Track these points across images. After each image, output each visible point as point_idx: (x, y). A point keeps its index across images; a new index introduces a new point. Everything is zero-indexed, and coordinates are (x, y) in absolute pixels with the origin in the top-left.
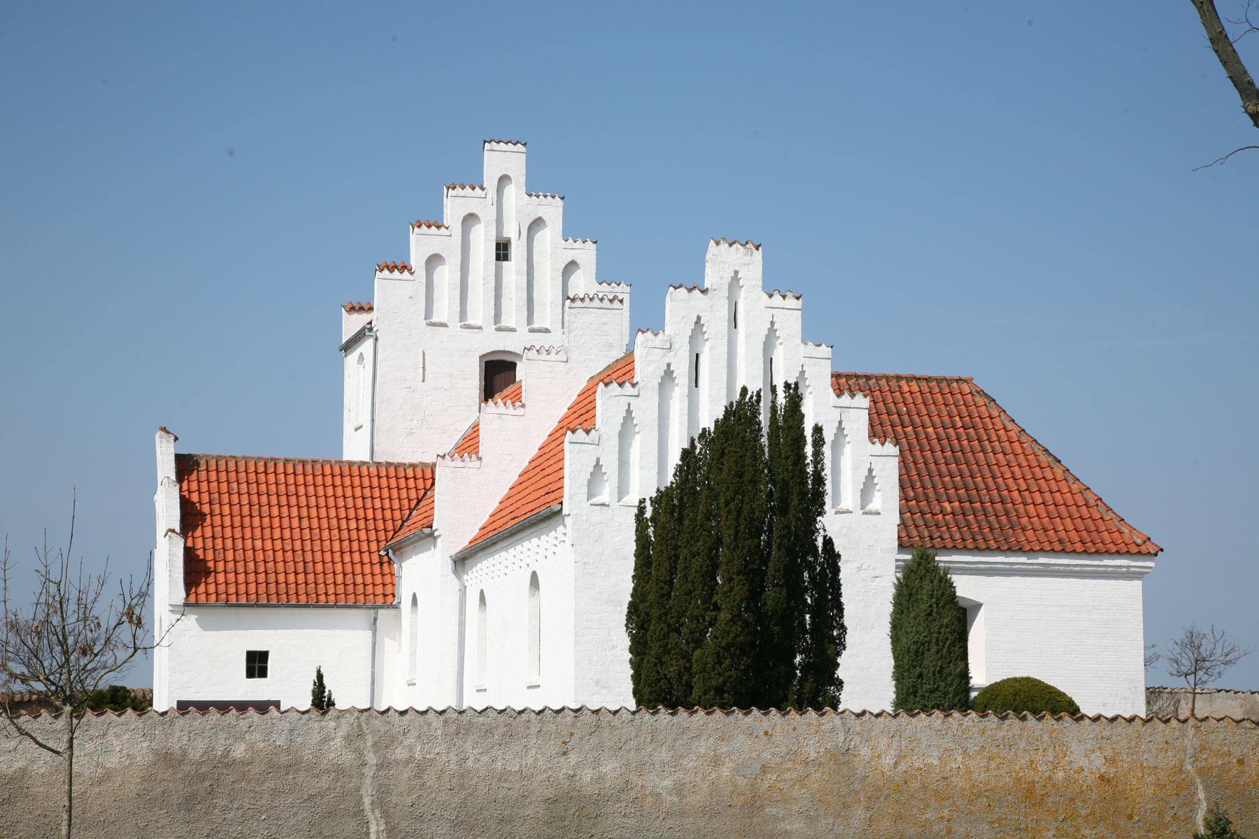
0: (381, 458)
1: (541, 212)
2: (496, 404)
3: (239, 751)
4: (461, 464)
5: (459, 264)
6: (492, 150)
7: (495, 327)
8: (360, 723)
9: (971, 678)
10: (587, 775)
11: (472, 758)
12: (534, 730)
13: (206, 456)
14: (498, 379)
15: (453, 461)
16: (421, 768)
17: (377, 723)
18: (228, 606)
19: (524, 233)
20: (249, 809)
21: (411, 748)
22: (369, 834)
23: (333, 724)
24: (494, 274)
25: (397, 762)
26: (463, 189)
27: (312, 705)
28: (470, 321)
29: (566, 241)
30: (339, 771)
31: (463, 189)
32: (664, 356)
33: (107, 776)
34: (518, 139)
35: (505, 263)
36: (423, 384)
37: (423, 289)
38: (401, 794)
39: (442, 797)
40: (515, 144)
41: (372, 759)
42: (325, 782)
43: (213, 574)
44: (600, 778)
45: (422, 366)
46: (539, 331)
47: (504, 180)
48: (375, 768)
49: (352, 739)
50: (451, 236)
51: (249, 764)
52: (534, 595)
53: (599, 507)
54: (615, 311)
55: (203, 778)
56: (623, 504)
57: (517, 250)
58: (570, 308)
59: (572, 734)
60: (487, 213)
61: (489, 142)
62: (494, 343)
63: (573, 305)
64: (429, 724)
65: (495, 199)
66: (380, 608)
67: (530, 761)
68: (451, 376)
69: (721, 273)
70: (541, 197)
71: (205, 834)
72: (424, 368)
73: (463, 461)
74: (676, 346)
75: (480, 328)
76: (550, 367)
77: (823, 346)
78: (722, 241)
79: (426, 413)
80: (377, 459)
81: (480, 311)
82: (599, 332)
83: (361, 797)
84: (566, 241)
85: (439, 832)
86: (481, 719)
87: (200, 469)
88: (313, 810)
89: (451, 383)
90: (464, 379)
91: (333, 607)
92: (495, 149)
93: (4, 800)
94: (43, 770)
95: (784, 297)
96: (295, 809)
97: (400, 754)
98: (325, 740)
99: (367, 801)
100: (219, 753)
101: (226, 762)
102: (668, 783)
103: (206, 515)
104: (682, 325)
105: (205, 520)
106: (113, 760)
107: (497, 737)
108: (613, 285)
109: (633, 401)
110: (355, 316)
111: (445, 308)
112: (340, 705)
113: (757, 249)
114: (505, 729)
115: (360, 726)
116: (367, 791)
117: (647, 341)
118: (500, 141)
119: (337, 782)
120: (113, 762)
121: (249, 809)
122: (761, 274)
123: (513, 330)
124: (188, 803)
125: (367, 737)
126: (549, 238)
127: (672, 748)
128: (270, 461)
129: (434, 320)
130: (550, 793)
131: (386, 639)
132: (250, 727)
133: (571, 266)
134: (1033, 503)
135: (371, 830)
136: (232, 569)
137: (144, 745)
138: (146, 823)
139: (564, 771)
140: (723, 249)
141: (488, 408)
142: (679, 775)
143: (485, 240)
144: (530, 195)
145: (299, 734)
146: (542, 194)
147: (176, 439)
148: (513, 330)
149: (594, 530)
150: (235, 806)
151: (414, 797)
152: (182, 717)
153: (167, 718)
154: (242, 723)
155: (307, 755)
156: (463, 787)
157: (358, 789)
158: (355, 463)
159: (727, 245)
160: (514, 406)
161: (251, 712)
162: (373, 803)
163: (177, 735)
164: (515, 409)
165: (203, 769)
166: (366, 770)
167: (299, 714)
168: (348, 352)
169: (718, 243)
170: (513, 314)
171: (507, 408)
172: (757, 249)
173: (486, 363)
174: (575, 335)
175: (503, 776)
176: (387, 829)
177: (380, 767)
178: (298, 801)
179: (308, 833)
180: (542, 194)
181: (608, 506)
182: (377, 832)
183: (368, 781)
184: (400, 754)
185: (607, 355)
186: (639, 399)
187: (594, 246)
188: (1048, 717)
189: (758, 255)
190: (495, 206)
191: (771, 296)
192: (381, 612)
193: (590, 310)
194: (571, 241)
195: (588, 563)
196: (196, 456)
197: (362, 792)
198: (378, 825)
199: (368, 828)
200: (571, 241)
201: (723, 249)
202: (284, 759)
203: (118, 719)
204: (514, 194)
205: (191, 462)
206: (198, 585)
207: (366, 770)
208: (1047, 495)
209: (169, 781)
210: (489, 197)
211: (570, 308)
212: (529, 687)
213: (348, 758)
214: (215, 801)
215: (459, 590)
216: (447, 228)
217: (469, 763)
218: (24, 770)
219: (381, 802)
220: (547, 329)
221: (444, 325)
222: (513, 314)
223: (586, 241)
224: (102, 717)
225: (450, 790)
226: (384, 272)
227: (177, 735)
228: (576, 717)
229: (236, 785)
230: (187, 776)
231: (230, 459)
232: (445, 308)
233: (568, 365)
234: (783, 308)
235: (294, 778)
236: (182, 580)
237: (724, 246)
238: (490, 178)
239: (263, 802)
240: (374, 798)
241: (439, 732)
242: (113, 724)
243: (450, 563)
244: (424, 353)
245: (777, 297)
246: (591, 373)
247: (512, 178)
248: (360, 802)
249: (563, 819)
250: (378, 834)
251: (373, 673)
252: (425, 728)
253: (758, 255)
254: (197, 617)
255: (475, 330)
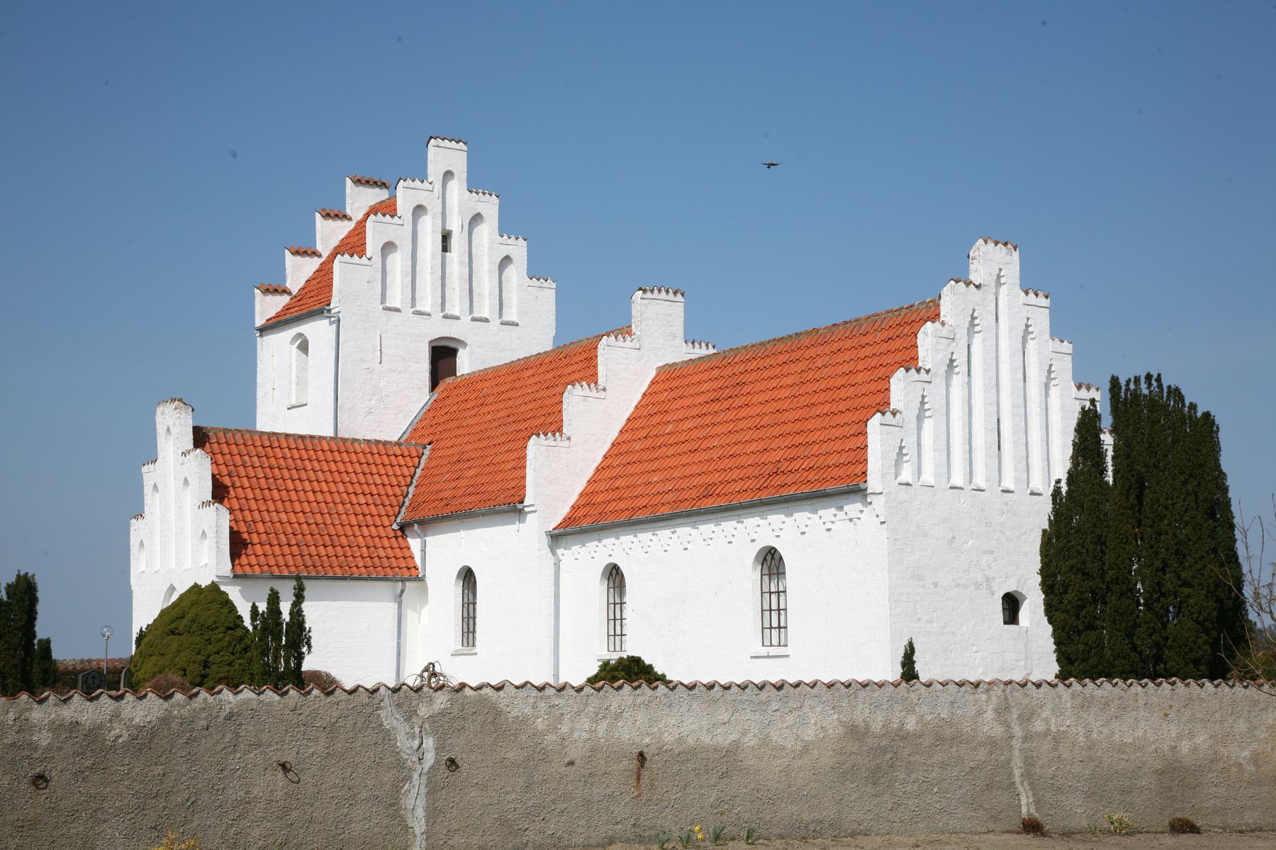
0: (343, 434)
1: (480, 208)
2: (582, 386)
3: (911, 724)
4: (554, 443)
5: (411, 252)
6: (438, 146)
7: (442, 314)
8: (1005, 696)
9: (1054, 652)
10: (1185, 746)
11: (1095, 730)
12: (1141, 703)
13: (214, 429)
14: (442, 364)
15: (546, 440)
16: (1057, 739)
17: (1019, 694)
18: (273, 578)
19: (466, 228)
20: (923, 782)
21: (1047, 720)
22: (1021, 806)
23: (984, 697)
24: (440, 264)
25: (1038, 735)
26: (413, 181)
27: (902, 677)
28: (448, 311)
29: (502, 237)
30: (992, 743)
31: (413, 181)
32: (949, 345)
33: (807, 748)
34: (438, 135)
35: (448, 254)
36: (380, 366)
37: (379, 275)
38: (1042, 767)
39: (1077, 768)
40: (457, 142)
41: (1018, 731)
42: (982, 754)
43: (250, 546)
44: (1195, 749)
45: (379, 348)
46: (480, 320)
47: (448, 175)
48: (1020, 740)
49: (1003, 710)
50: (403, 225)
51: (920, 737)
52: (756, 569)
53: (904, 487)
54: (678, 303)
55: (884, 750)
56: (922, 484)
57: (457, 242)
58: (642, 298)
59: (1171, 707)
60: (434, 206)
61: (435, 139)
62: (441, 329)
63: (645, 296)
64: (1060, 697)
65: (441, 193)
66: (408, 580)
67: (1141, 733)
68: (405, 359)
69: (990, 270)
70: (481, 194)
71: (890, 808)
72: (381, 350)
73: (555, 440)
74: (958, 336)
75: (429, 315)
76: (626, 353)
77: (1066, 342)
78: (989, 241)
79: (384, 393)
80: (340, 435)
81: (427, 302)
82: (665, 323)
83: (1012, 769)
84: (502, 237)
85: (1076, 804)
86: (1100, 691)
87: (211, 441)
88: (974, 782)
89: (405, 366)
90: (416, 362)
91: (367, 580)
92: (441, 145)
93: (723, 773)
94: (752, 743)
95: (1037, 295)
96: (960, 782)
97: (1039, 726)
98: (980, 713)
99: (1017, 772)
100: (896, 726)
101: (904, 737)
102: (1246, 753)
103: (229, 487)
104: (962, 317)
105: (228, 492)
106: (809, 732)
107: (1113, 710)
108: (542, 280)
109: (927, 386)
110: (270, 298)
111: (397, 297)
112: (924, 677)
113: (1015, 250)
114: (1119, 702)
115: (1006, 699)
116: (1017, 763)
117: (937, 330)
118: (445, 139)
119: (991, 754)
120: (809, 734)
121: (923, 782)
122: (1018, 273)
123: (457, 318)
124: (875, 776)
125: (1012, 710)
126: (487, 231)
127: (1248, 720)
128: (272, 435)
129: (388, 305)
130: (1158, 765)
131: (408, 610)
132: (919, 699)
133: (506, 260)
134: (290, 500)
135: (1022, 803)
136: (266, 541)
137: (834, 718)
138: (841, 798)
139: (1167, 743)
140: (990, 248)
141: (575, 390)
142: (1254, 746)
143: (432, 231)
144: (471, 192)
145: (958, 707)
146: (481, 191)
147: (193, 410)
148: (457, 318)
149: (902, 508)
150: (912, 779)
151: (1053, 768)
152: (864, 690)
153: (851, 690)
154: (912, 695)
155: (966, 728)
156: (1091, 760)
157: (1009, 762)
158: (348, 439)
159: (993, 244)
160: (597, 389)
161: (967, 688)
162: (1022, 775)
163: (860, 708)
164: (598, 392)
165: (884, 743)
166: (1014, 742)
167: (957, 687)
168: (264, 333)
169: (986, 242)
170: (456, 306)
171: (591, 391)
172: (1015, 250)
173: (433, 347)
174: (646, 324)
175: (1121, 748)
176: (1034, 801)
177: (1025, 739)
178: (962, 774)
179: (971, 806)
180: (481, 191)
181: (911, 485)
182: (1028, 804)
183: (1016, 753)
184: (1039, 726)
185: (672, 345)
186: (931, 385)
187: (525, 243)
188: (644, 685)
189: (1016, 255)
190: (441, 200)
191: (1027, 293)
192: (408, 584)
193: (658, 301)
194: (506, 237)
195: (898, 539)
196: (205, 428)
197: (1013, 764)
198: (1027, 797)
199: (1019, 800)
200: (506, 237)
201: (990, 248)
202: (948, 732)
203: (812, 690)
204: (457, 188)
205: (201, 434)
206: (239, 556)
207: (1014, 742)
208: (258, 491)
209: (857, 754)
210: (436, 190)
211: (642, 298)
212: (752, 657)
213: (998, 730)
214: (895, 774)
215: (554, 564)
216: (400, 218)
217: (1095, 735)
218: (736, 743)
219: (1027, 775)
220: (487, 319)
221: (397, 310)
222: (456, 306)
223: (518, 238)
224: (798, 689)
225: (1082, 762)
226: (345, 256)
227: (860, 708)
228: (1173, 690)
229: (912, 759)
230: (872, 749)
231: (236, 432)
232: (397, 297)
233: (640, 353)
234: (1036, 306)
235: (957, 751)
236: (229, 552)
237: (991, 245)
238: (435, 169)
239: (934, 774)
240: (1023, 770)
241: (1069, 705)
242: (808, 696)
243: (545, 540)
244: (380, 336)
245: (1031, 295)
246: (499, 362)
247: (455, 174)
248: (1011, 775)
249: (1170, 789)
250: (1028, 806)
251: (399, 644)
252: (1057, 700)
253: (1016, 255)
254: (240, 588)
255: (425, 317)
